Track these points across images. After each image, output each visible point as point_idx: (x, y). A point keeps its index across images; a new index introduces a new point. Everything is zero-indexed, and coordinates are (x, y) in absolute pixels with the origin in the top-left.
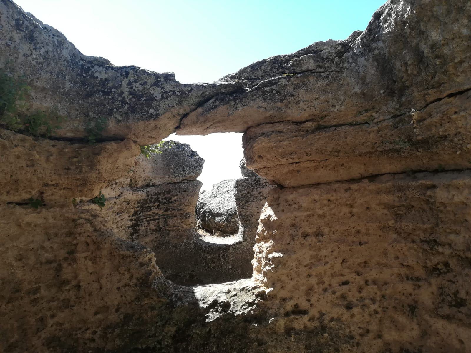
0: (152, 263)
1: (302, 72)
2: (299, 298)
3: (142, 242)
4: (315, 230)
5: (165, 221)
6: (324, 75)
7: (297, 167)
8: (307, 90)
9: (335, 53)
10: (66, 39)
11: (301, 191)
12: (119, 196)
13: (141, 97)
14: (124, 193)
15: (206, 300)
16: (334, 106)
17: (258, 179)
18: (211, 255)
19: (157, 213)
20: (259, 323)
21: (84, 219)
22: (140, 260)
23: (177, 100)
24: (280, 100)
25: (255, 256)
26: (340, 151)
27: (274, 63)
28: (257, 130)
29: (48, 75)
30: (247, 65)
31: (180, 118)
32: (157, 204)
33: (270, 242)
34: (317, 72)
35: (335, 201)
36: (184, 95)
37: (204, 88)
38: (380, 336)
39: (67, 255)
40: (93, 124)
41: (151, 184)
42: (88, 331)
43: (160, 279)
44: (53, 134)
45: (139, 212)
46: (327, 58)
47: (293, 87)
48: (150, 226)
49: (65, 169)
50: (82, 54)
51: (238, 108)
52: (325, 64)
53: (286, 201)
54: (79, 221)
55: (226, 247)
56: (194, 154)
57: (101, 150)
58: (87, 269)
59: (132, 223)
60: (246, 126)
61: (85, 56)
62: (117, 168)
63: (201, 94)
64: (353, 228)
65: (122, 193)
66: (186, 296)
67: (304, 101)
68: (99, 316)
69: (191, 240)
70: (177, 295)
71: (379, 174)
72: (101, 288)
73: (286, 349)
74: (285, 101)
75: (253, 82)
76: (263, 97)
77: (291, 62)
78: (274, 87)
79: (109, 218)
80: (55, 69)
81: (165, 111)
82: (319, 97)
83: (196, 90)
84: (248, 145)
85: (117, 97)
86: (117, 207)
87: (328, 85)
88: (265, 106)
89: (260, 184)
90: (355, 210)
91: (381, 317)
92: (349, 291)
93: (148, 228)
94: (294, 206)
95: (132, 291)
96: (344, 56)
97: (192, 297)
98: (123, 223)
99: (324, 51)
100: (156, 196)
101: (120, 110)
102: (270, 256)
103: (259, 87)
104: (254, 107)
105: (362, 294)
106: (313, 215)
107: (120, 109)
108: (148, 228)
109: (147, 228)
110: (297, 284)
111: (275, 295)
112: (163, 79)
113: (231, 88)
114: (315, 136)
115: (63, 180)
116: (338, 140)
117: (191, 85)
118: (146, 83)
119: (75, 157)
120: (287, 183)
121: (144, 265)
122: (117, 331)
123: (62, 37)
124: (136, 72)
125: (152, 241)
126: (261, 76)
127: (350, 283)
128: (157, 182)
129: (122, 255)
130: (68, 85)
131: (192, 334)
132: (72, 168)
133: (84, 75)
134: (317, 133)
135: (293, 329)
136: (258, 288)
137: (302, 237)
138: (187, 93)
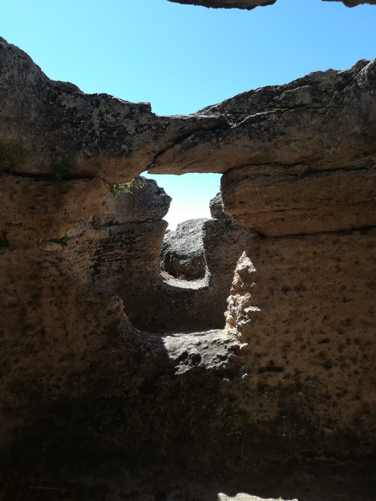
0: (120, 311)
1: (295, 107)
2: (274, 355)
3: (104, 282)
4: (297, 284)
5: (127, 262)
6: (320, 111)
7: (282, 215)
8: (300, 128)
9: (335, 86)
10: (32, 61)
11: (284, 241)
12: (81, 235)
13: (113, 130)
14: (87, 232)
15: (176, 352)
16: (329, 147)
17: (229, 221)
18: (175, 299)
19: (120, 254)
20: (231, 378)
21: (49, 262)
22: (109, 308)
23: (153, 135)
24: (269, 138)
25: (228, 307)
26: (331, 199)
27: (263, 95)
28: (240, 172)
29: (13, 102)
30: (231, 96)
31: (154, 155)
32: (120, 243)
33: (247, 295)
34: (313, 108)
35: (321, 254)
36: (160, 130)
37: (183, 122)
38: (358, 398)
39: (31, 299)
40: (60, 159)
41: (114, 222)
42: (53, 378)
43: (128, 328)
44: (17, 170)
45: (101, 252)
46: (325, 91)
47: (284, 124)
48: (112, 266)
49: (30, 208)
50: (48, 78)
51: (221, 147)
52: (323, 98)
53: (267, 252)
54: (44, 264)
55: (191, 292)
56: (161, 191)
57: (69, 189)
58: (52, 314)
59: (93, 263)
60: (228, 167)
61: (52, 81)
62: (84, 209)
63: (180, 129)
64: (339, 283)
65: (84, 232)
66: (154, 346)
67: (295, 141)
68: (64, 363)
69: (155, 283)
70: (145, 345)
71: (372, 226)
72: (67, 335)
73: (258, 406)
74: (274, 141)
75: (238, 117)
76: (249, 135)
77: (283, 95)
78: (263, 123)
79: (71, 258)
80: (21, 97)
81: (139, 147)
82: (313, 137)
83: (174, 125)
84: (229, 189)
85: (86, 129)
86: (79, 246)
87: (324, 123)
88: (251, 145)
89: (230, 227)
90: (342, 265)
91: (361, 378)
92: (329, 349)
93: (110, 269)
94: (275, 257)
95: (99, 339)
96: (345, 89)
97: (161, 348)
98: (85, 263)
99: (323, 83)
100: (119, 236)
101: (90, 145)
102: (247, 310)
103: (245, 123)
104: (239, 146)
105: (342, 354)
106: (296, 268)
107: (90, 143)
108: (110, 269)
109: (108, 269)
110: (274, 340)
111: (250, 351)
112: (137, 111)
113: (213, 123)
114: (305, 181)
115: (28, 220)
116: (330, 187)
117: (168, 118)
118: (118, 114)
119: (40, 195)
120: (269, 232)
121: (113, 313)
122: (83, 379)
123: (28, 59)
124: (107, 101)
125: (114, 283)
126: (247, 110)
127: (330, 342)
128: (120, 220)
129: (89, 302)
130: (34, 115)
131: (161, 386)
132: (37, 207)
133: (51, 103)
134: (307, 178)
135: (267, 385)
136: (231, 342)
137: (282, 291)
138: (164, 127)
